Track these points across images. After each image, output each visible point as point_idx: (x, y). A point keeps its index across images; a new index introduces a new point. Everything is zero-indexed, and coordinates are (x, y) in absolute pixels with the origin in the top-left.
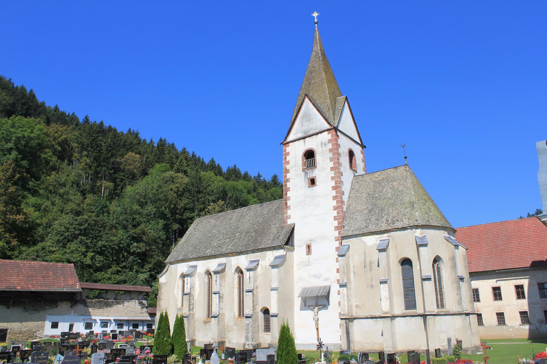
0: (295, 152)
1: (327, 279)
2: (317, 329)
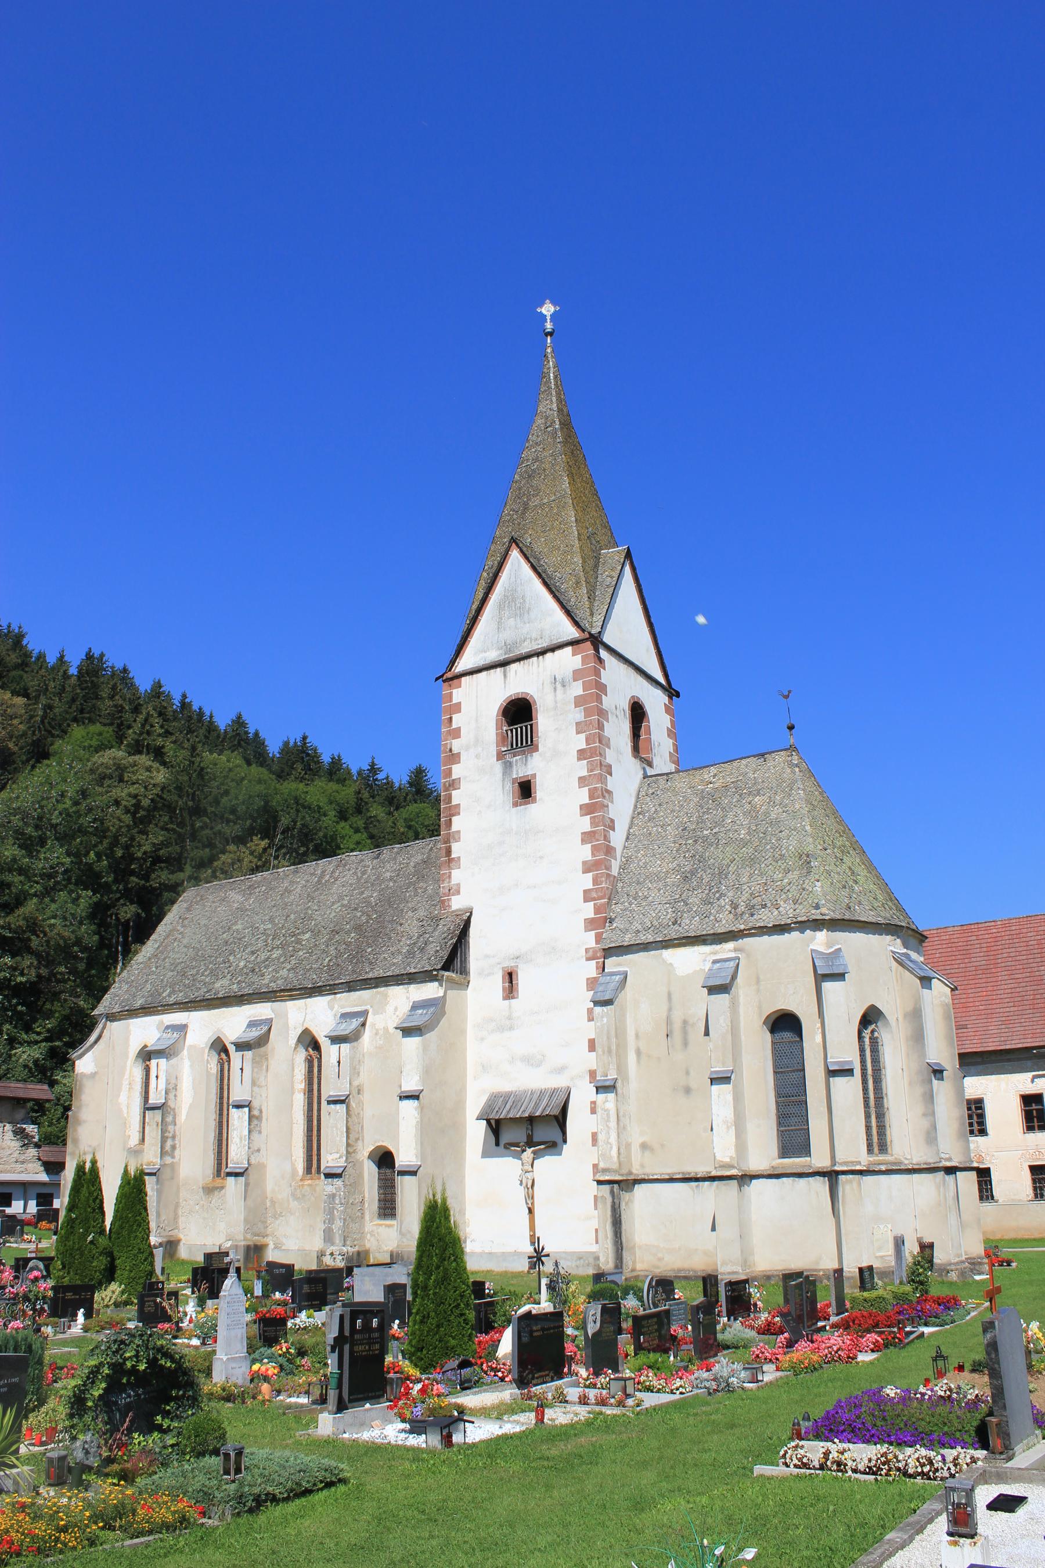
0: (478, 703)
1: (561, 1070)
2: (531, 1211)
